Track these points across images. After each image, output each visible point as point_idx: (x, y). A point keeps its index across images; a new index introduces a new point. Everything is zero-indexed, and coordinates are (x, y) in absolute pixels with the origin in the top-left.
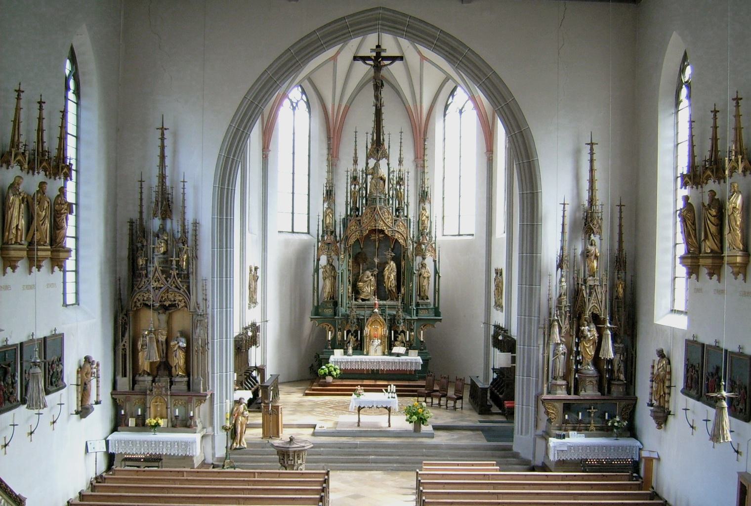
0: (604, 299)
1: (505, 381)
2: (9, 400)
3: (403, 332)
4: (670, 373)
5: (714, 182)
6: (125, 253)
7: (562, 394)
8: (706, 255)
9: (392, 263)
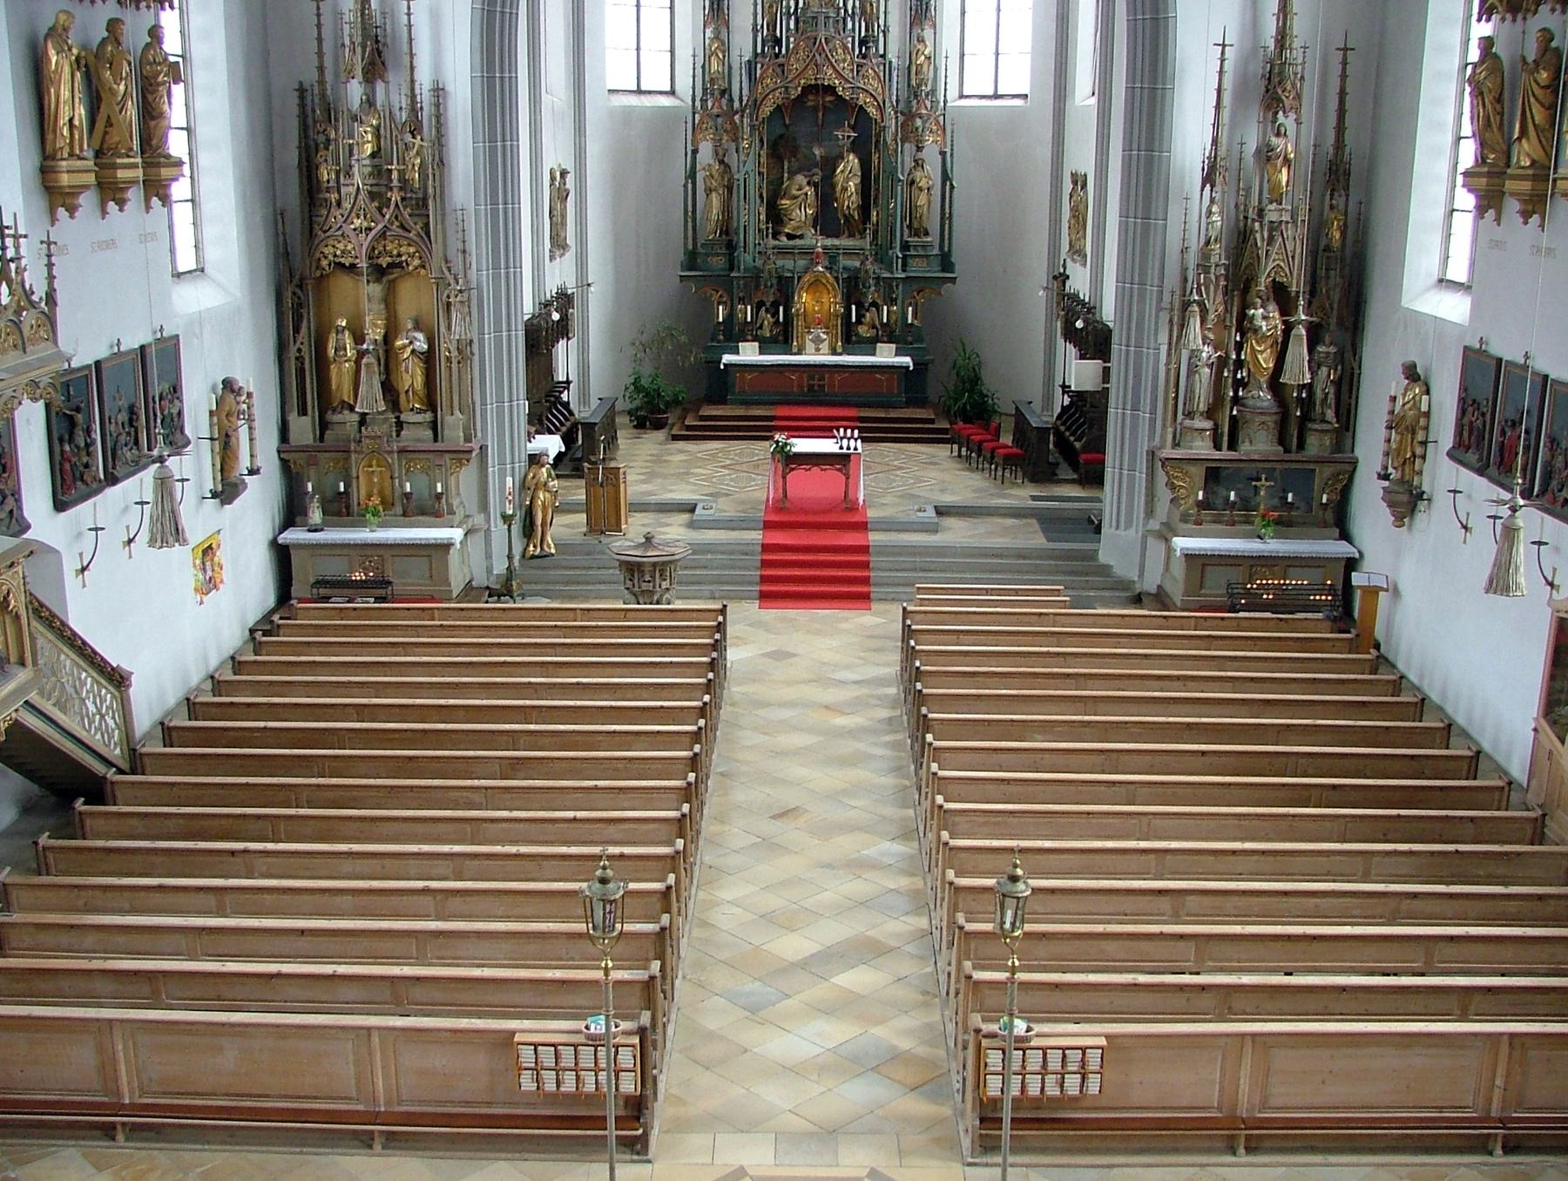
0: (1298, 251)
1: (1086, 412)
2: (82, 480)
3: (874, 304)
4: (1427, 415)
5: (1553, 10)
6: (293, 157)
7: (1202, 448)
8: (1520, 171)
9: (851, 157)
